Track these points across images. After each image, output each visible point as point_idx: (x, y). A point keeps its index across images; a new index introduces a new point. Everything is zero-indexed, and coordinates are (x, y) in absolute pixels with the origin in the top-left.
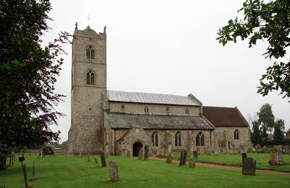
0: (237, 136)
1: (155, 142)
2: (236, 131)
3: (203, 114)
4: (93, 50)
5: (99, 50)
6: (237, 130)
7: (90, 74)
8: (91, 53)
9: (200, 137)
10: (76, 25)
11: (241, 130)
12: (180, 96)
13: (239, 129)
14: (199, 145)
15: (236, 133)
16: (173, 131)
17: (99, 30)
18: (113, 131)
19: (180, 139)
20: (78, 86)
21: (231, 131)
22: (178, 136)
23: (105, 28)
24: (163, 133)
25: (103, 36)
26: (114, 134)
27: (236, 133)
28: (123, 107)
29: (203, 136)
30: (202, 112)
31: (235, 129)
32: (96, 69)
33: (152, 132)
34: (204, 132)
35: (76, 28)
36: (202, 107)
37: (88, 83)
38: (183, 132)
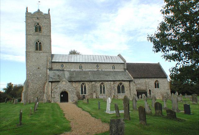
0: (157, 85)
1: (84, 91)
2: (156, 81)
3: (127, 69)
4: (40, 26)
5: (44, 26)
6: (157, 81)
7: (38, 43)
8: (38, 29)
9: (121, 87)
10: (27, 9)
11: (160, 81)
12: (111, 57)
13: (158, 80)
14: (120, 93)
15: (157, 83)
16: (98, 82)
17: (45, 11)
18: (50, 83)
19: (104, 88)
20: (29, 52)
21: (152, 82)
22: (102, 86)
23: (49, 10)
24: (90, 84)
25: (47, 17)
26: (51, 86)
27: (157, 83)
28: (62, 66)
29: (123, 85)
30: (126, 67)
31: (155, 80)
32: (42, 40)
33: (81, 83)
34: (123, 83)
35: (27, 11)
36: (126, 64)
37: (37, 49)
38: (106, 83)
